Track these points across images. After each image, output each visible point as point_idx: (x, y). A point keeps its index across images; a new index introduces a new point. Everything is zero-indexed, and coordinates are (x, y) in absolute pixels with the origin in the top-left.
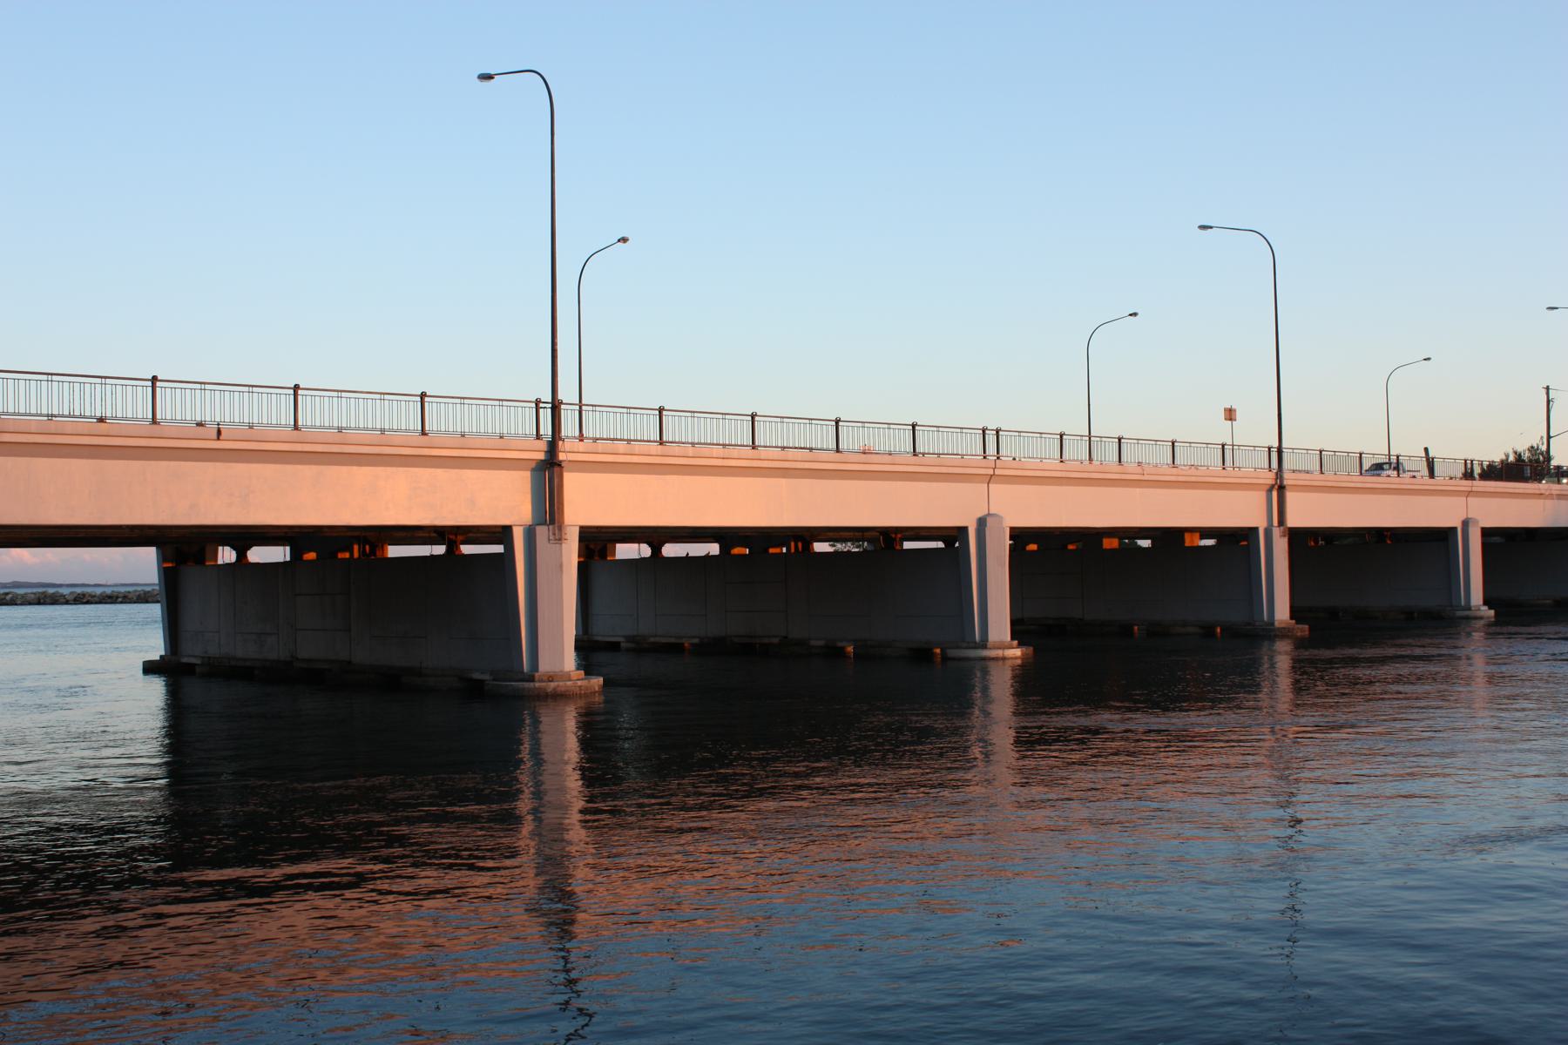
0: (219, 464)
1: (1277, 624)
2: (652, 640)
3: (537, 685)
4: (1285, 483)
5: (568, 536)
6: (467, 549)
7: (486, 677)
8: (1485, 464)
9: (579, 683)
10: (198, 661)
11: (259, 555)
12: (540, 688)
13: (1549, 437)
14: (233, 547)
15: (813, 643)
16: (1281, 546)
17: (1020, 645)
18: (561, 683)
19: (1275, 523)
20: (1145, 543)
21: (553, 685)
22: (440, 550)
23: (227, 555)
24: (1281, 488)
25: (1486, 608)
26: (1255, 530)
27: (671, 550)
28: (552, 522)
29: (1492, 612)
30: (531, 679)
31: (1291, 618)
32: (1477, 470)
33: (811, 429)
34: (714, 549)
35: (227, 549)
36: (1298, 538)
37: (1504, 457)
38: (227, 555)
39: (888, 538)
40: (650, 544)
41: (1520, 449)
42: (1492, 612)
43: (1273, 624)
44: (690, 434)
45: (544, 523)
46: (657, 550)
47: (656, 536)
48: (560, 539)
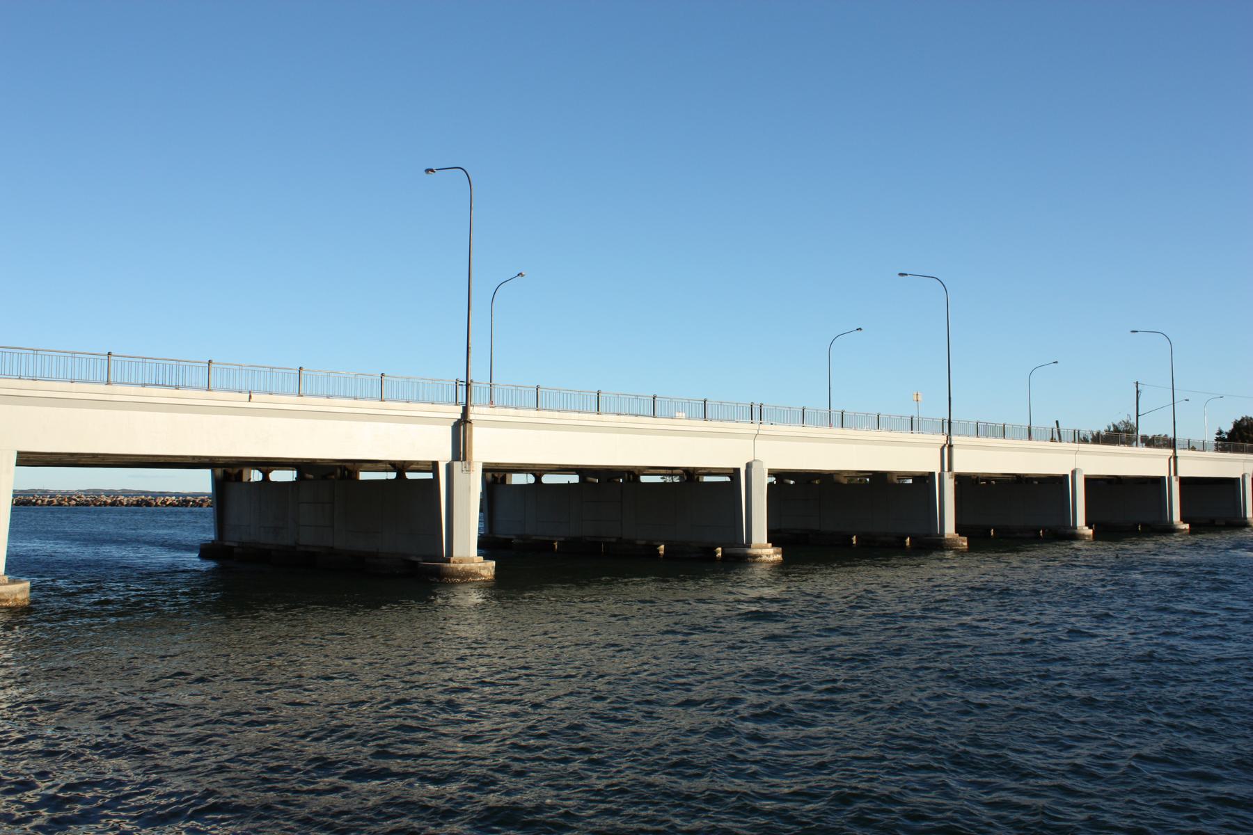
0: (250, 418)
1: (946, 536)
2: (534, 538)
3: (452, 565)
4: (953, 443)
5: (474, 469)
6: (409, 476)
7: (419, 559)
8: (1095, 433)
9: (479, 565)
10: (236, 545)
11: (277, 476)
12: (452, 568)
13: (1138, 415)
14: (260, 470)
15: (638, 542)
16: (950, 485)
17: (773, 546)
18: (468, 565)
19: (946, 469)
20: (1036, 483)
21: (462, 565)
22: (392, 475)
23: (256, 476)
24: (950, 446)
25: (1087, 528)
26: (932, 474)
27: (547, 479)
28: (465, 459)
29: (1090, 532)
30: (448, 561)
31: (956, 532)
32: (1090, 437)
33: (637, 402)
34: (575, 479)
35: (257, 471)
36: (1184, 482)
37: (1107, 428)
38: (256, 476)
39: (690, 475)
40: (534, 475)
41: (1116, 423)
42: (1090, 532)
43: (943, 536)
44: (167, 376)
45: (458, 459)
46: (538, 479)
47: (538, 471)
48: (469, 471)
